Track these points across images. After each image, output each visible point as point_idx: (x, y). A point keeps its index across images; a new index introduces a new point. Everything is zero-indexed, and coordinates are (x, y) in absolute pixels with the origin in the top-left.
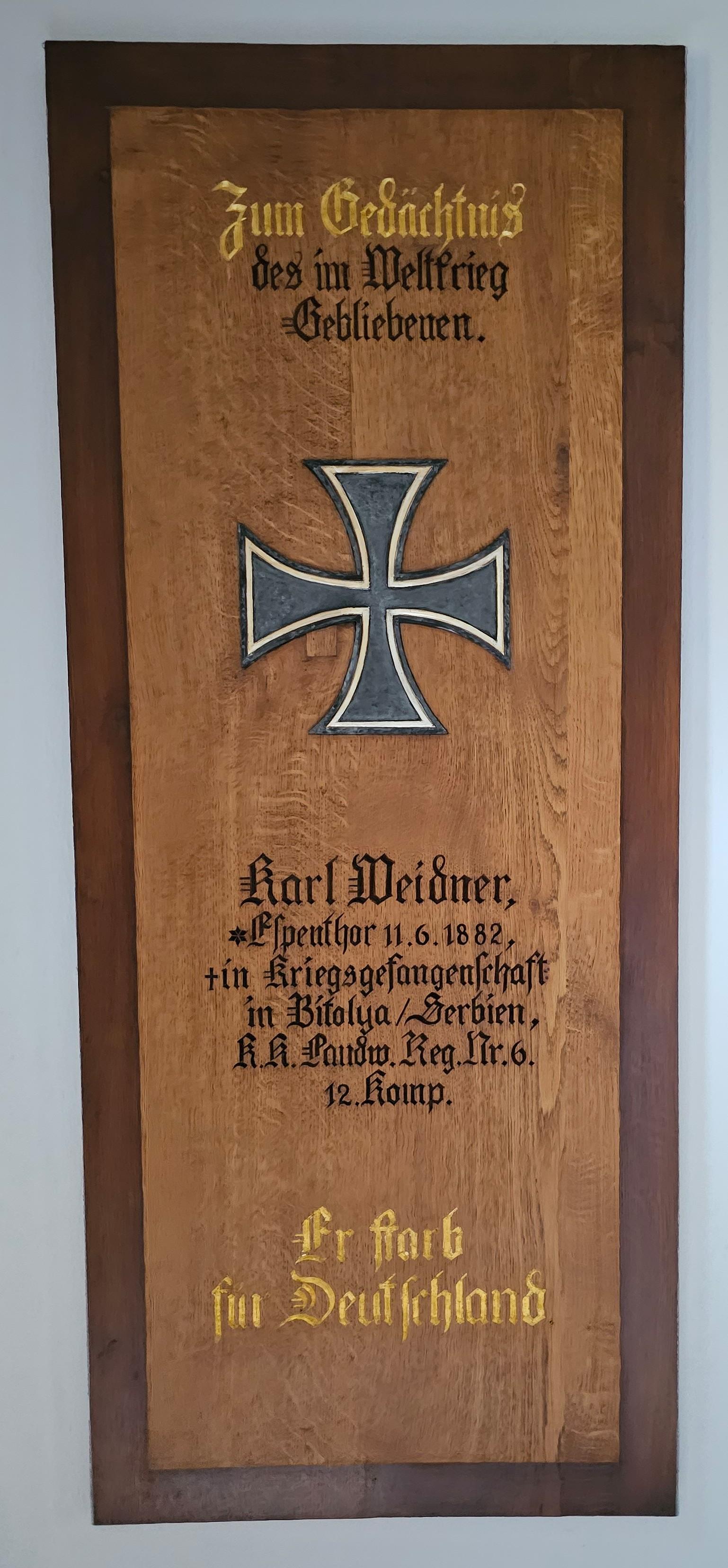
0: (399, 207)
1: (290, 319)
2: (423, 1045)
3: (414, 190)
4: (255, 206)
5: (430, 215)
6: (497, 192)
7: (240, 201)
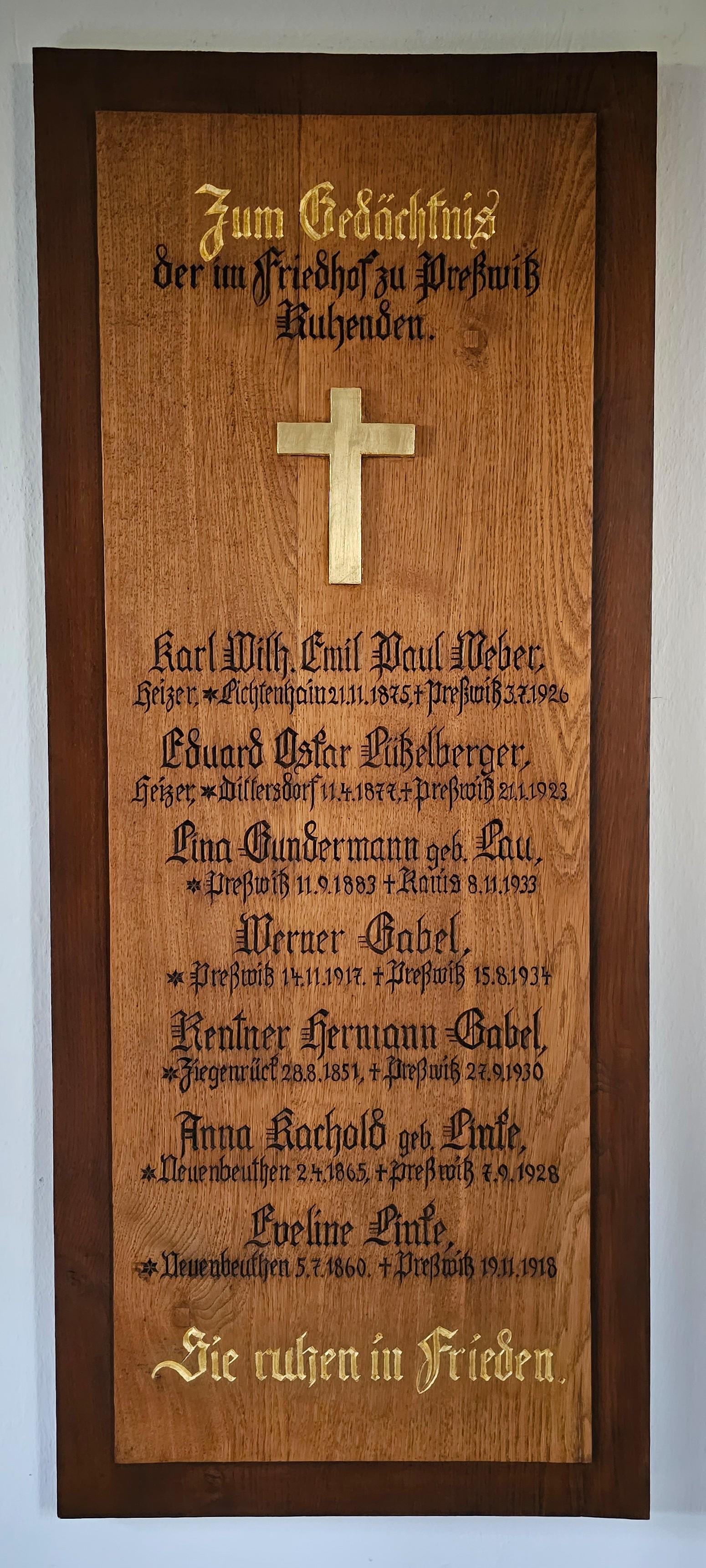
0: (516, 1352)
1: (376, 1224)
2: (198, 1026)
3: (392, 196)
4: (236, 211)
5: (406, 219)
6: (469, 194)
7: (225, 202)
